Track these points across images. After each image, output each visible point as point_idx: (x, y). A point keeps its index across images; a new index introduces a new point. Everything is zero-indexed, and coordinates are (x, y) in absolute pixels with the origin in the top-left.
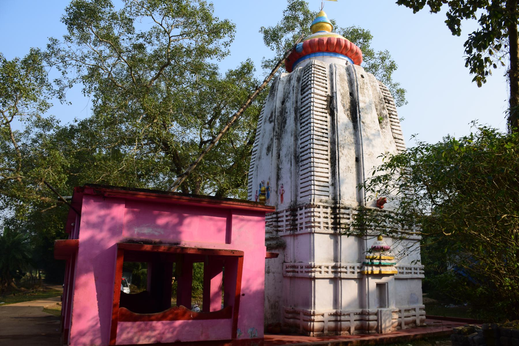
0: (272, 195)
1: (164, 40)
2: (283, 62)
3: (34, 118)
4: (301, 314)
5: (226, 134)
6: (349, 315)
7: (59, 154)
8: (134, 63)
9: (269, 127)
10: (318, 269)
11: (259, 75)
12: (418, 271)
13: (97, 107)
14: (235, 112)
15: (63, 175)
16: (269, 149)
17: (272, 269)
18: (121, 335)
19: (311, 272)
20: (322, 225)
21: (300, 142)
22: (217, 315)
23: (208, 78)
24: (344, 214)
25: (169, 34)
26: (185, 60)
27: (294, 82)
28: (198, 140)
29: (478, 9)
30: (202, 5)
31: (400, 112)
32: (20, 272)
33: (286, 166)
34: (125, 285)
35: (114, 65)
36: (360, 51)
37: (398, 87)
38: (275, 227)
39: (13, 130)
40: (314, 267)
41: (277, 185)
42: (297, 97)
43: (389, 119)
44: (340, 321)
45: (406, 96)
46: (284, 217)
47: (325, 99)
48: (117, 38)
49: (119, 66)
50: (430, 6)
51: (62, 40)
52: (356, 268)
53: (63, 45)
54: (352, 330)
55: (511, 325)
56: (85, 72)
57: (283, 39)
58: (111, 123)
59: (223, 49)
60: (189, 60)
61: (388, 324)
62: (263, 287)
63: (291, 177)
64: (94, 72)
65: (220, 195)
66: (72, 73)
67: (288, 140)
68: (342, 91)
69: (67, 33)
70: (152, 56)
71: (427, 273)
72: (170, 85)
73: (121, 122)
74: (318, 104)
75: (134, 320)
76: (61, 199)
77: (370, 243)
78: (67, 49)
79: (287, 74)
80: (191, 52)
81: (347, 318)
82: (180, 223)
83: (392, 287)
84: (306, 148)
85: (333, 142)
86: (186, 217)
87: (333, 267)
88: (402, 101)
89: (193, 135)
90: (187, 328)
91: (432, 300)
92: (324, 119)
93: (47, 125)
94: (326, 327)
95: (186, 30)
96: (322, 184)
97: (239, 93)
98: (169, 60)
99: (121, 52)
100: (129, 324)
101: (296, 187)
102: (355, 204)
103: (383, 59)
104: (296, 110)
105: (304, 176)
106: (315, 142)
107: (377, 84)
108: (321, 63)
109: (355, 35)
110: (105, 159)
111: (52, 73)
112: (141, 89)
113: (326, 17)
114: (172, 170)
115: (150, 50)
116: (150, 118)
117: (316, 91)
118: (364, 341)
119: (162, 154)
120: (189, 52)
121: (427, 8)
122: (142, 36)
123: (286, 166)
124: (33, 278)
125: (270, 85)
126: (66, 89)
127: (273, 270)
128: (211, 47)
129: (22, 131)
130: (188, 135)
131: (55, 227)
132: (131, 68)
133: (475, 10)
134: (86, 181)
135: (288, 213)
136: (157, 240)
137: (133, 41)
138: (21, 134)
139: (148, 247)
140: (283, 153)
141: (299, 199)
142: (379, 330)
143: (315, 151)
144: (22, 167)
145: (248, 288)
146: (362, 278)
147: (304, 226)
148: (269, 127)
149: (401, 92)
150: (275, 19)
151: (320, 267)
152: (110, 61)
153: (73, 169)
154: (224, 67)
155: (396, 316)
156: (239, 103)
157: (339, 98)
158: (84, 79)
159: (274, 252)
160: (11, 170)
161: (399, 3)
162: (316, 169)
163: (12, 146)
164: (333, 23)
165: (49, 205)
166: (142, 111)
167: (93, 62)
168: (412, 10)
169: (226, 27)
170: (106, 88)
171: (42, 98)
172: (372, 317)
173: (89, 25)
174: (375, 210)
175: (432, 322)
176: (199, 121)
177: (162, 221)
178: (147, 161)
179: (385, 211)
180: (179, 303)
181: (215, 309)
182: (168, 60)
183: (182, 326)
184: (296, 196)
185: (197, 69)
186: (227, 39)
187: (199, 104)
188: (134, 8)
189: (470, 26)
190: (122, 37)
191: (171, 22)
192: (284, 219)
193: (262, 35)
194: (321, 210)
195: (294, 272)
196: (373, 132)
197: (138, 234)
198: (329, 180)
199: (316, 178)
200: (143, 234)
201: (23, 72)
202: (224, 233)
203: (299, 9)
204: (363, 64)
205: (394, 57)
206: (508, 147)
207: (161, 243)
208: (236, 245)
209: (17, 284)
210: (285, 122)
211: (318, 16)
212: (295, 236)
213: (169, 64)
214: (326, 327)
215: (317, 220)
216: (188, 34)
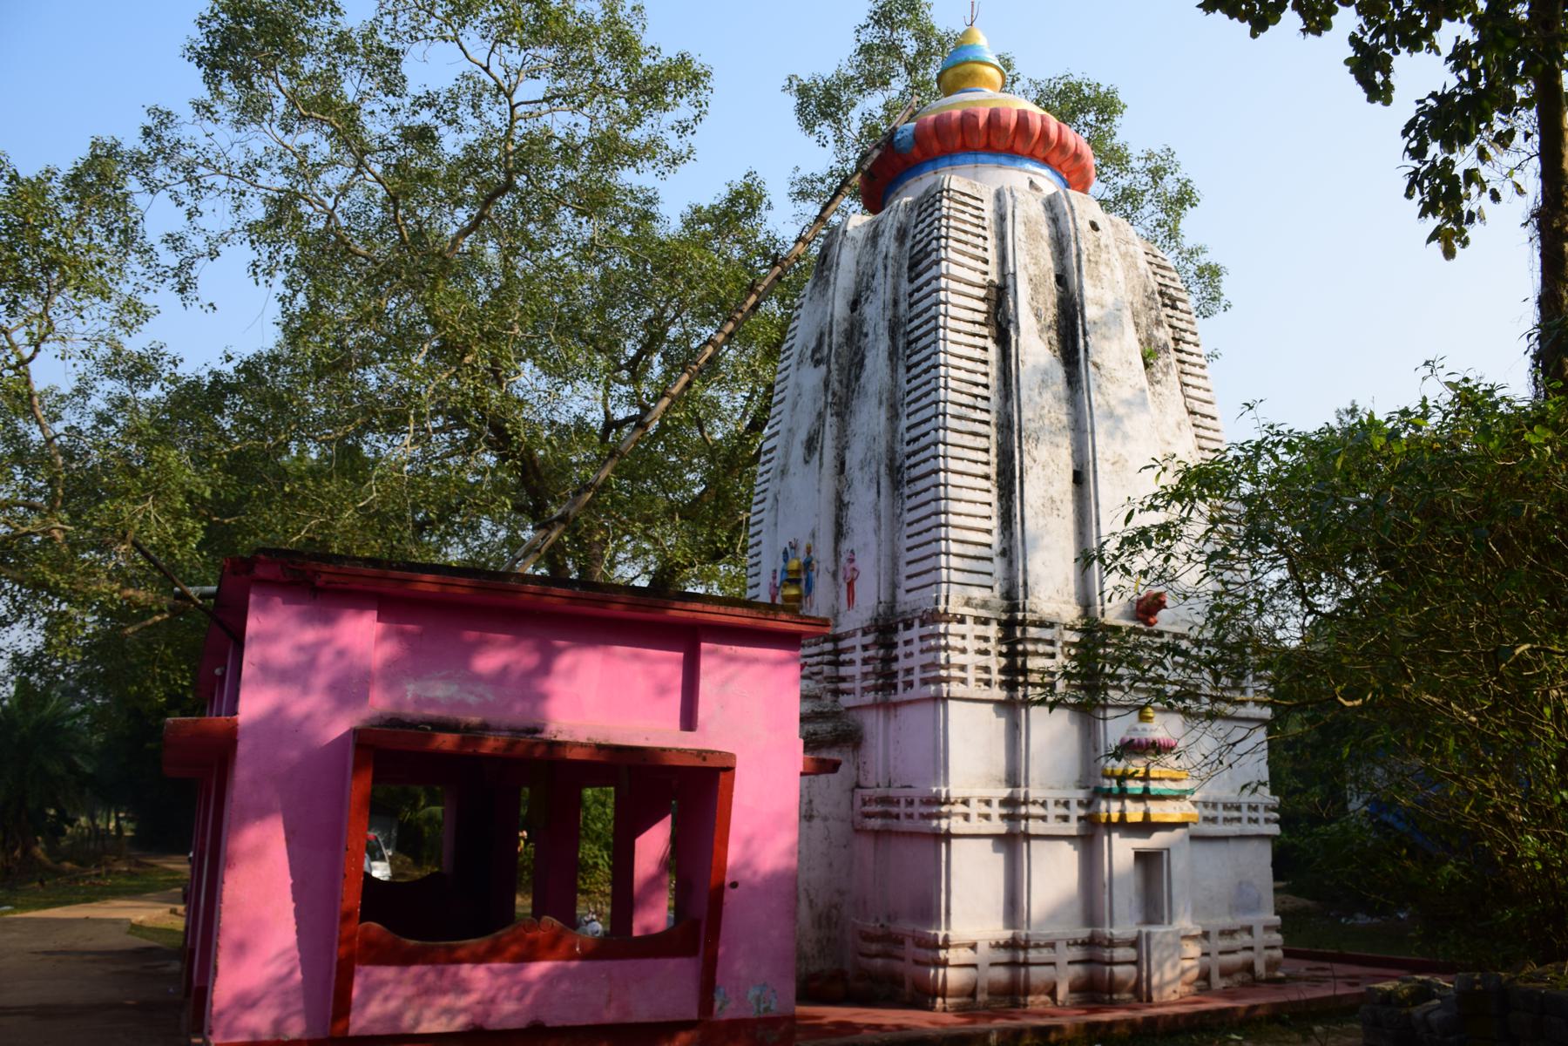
2: (856, 181)
3: (104, 351)
4: (909, 943)
6: (1052, 945)
7: (177, 457)
8: (405, 184)
9: (811, 377)
10: (960, 808)
11: (783, 221)
12: (1261, 814)
14: (709, 331)
15: (189, 523)
16: (811, 445)
17: (820, 808)
18: (364, 1005)
19: (939, 816)
20: (971, 675)
21: (904, 423)
22: (655, 946)
23: (626, 231)
24: (1037, 641)
25: (509, 96)
26: (558, 175)
27: (888, 243)
28: (596, 418)
31: (1207, 333)
32: (61, 813)
33: (864, 498)
34: (376, 856)
35: (344, 191)
36: (1087, 151)
37: (1203, 260)
38: (830, 679)
40: (947, 801)
41: (837, 553)
42: (896, 288)
43: (1174, 356)
44: (1026, 964)
45: (1227, 285)
46: (858, 650)
47: (982, 293)
48: (354, 108)
49: (357, 194)
50: (1302, 14)
51: (186, 113)
52: (1073, 804)
53: (190, 129)
54: (1062, 991)
55: (1541, 978)
57: (855, 114)
59: (673, 142)
60: (571, 175)
61: (1169, 973)
62: (794, 862)
63: (877, 531)
64: (283, 209)
65: (665, 583)
66: (217, 214)
67: (870, 418)
68: (1032, 270)
69: (204, 93)
72: (514, 251)
73: (365, 363)
74: (960, 308)
75: (404, 959)
76: (183, 596)
77: (1117, 728)
78: (202, 142)
79: (868, 218)
80: (576, 150)
81: (1045, 955)
82: (545, 669)
83: (1183, 864)
84: (923, 442)
85: (1007, 427)
86: (561, 651)
87: (1004, 803)
88: (1212, 300)
89: (582, 402)
90: (565, 986)
91: (1301, 902)
92: (978, 354)
93: (141, 369)
94: (983, 983)
95: (562, 83)
96: (971, 550)
97: (722, 276)
98: (509, 174)
100: (388, 973)
101: (894, 559)
102: (1070, 612)
103: (1156, 174)
104: (894, 328)
105: (916, 528)
106: (951, 423)
107: (1139, 248)
108: (971, 185)
109: (1072, 101)
110: (316, 473)
111: (157, 215)
112: (423, 263)
113: (985, 45)
114: (518, 509)
115: (451, 144)
118: (1098, 1024)
119: (490, 459)
120: (569, 152)
121: (1291, 19)
122: (429, 101)
123: (864, 498)
124: (100, 835)
125: (815, 250)
126: (200, 263)
127: (823, 810)
128: (638, 135)
130: (568, 400)
132: (394, 199)
133: (1435, 25)
134: (259, 540)
135: (870, 639)
136: (475, 719)
137: (401, 117)
138: (62, 398)
139: (447, 741)
140: (854, 457)
141: (901, 596)
142: (1141, 992)
143: (952, 451)
144: (69, 496)
145: (747, 864)
146: (1090, 835)
147: (916, 676)
148: (811, 377)
149: (1211, 274)
150: (830, 54)
151: (965, 802)
152: (333, 178)
153: (220, 505)
154: (677, 195)
155: (1193, 950)
156: (722, 304)
158: (256, 232)
159: (832, 755)
160: (32, 508)
163: (36, 436)
165: (146, 611)
166: (429, 330)
167: (281, 182)
168: (1247, 26)
169: (684, 77)
170: (321, 259)
171: (127, 289)
172: (1120, 953)
173: (268, 68)
174: (1133, 630)
175: (1301, 967)
176: (601, 360)
177: (489, 661)
178: (444, 480)
179: (1160, 634)
180: (539, 910)
181: (647, 929)
182: (506, 176)
183: (549, 979)
184: (894, 586)
185: (594, 201)
187: (601, 308)
188: (403, 18)
189: (1422, 75)
190: (368, 106)
191: (515, 59)
192: (858, 655)
193: (793, 101)
194: (970, 628)
195: (885, 815)
196: (1127, 393)
197: (417, 700)
198: (995, 539)
199: (953, 534)
200: (432, 702)
201: (68, 211)
202: (676, 699)
203: (903, 23)
204: (1097, 187)
205: (1190, 167)
206: (1534, 440)
207: (485, 727)
208: (712, 736)
210: (861, 365)
211: (962, 43)
212: (889, 707)
213: (509, 186)
214: (983, 983)
215: (956, 658)
216: (568, 97)
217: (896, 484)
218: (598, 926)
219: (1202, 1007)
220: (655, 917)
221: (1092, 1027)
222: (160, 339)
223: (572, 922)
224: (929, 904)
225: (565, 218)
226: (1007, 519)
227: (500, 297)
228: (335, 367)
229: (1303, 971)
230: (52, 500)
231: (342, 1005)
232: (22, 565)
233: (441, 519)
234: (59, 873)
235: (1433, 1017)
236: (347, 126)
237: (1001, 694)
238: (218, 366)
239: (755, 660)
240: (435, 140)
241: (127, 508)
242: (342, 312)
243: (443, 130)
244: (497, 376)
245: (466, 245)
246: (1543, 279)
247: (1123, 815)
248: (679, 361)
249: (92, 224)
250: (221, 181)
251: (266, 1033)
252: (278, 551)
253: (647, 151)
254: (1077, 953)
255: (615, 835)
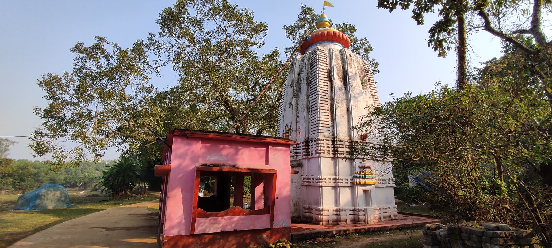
0: (293, 133)
2: (299, 48)
3: (141, 86)
4: (314, 210)
5: (264, 95)
6: (345, 211)
7: (157, 108)
8: (204, 51)
9: (290, 90)
10: (324, 180)
11: (283, 57)
13: (181, 79)
14: (268, 81)
17: (294, 181)
18: (198, 227)
19: (320, 182)
20: (326, 152)
21: (310, 99)
22: (260, 212)
23: (251, 60)
25: (225, 32)
27: (306, 61)
28: (245, 99)
29: (435, 5)
30: (246, 12)
34: (200, 191)
35: (191, 52)
39: (126, 95)
41: (296, 127)
42: (308, 71)
43: (368, 83)
46: (301, 147)
48: (193, 35)
49: (194, 53)
52: (349, 180)
53: (158, 39)
54: (348, 222)
56: (173, 56)
57: (298, 34)
59: (260, 41)
60: (239, 49)
61: (372, 218)
63: (305, 122)
66: (164, 56)
67: (303, 98)
69: (160, 31)
70: (215, 46)
71: (397, 183)
72: (227, 65)
73: (197, 88)
74: (322, 74)
75: (207, 216)
76: (159, 139)
78: (161, 41)
79: (301, 56)
82: (236, 153)
83: (374, 193)
85: (332, 99)
86: (240, 150)
87: (334, 179)
88: (376, 71)
89: (243, 96)
91: (399, 201)
92: (325, 84)
93: (149, 91)
94: (331, 219)
95: (237, 29)
97: (271, 69)
98: (226, 49)
99: (195, 44)
101: (309, 128)
102: (347, 138)
103: (363, 44)
105: (313, 121)
106: (320, 99)
108: (323, 48)
109: (349, 29)
111: (151, 56)
112: (208, 68)
113: (326, 17)
114: (230, 118)
115: (214, 42)
116: (215, 86)
117: (320, 66)
119: (224, 108)
120: (239, 44)
121: (399, 7)
122: (209, 33)
123: (302, 115)
124: (140, 188)
125: (290, 63)
126: (161, 67)
128: (253, 40)
130: (238, 95)
131: (155, 155)
135: (304, 144)
137: (203, 37)
138: (131, 97)
139: (216, 169)
140: (299, 107)
141: (310, 135)
142: (366, 222)
143: (320, 105)
144: (134, 117)
146: (353, 186)
147: (314, 152)
148: (290, 90)
150: (293, 21)
153: (167, 119)
154: (261, 53)
155: (377, 212)
158: (174, 60)
159: (297, 169)
160: (126, 120)
161: (381, 5)
162: (321, 116)
163: (126, 104)
164: (331, 21)
165: (151, 141)
166: (210, 81)
167: (178, 50)
168: (389, 10)
169: (262, 27)
170: (187, 67)
172: (361, 213)
174: (361, 142)
175: (402, 216)
176: (246, 87)
177: (225, 152)
178: (215, 113)
179: (367, 143)
180: (235, 204)
181: (258, 208)
182: (225, 48)
184: (309, 133)
185: (244, 54)
186: (262, 34)
187: (246, 76)
189: (433, 17)
192: (301, 148)
194: (325, 142)
195: (308, 182)
196: (358, 92)
198: (330, 123)
199: (321, 122)
203: (308, 14)
204: (350, 47)
205: (371, 42)
209: (131, 192)
210: (301, 87)
211: (322, 17)
212: (308, 159)
214: (331, 219)
215: (322, 148)
216: (238, 32)
217: (309, 112)
221: (356, 230)
224: (318, 202)
225: (238, 57)
226: (332, 119)
227: (225, 75)
228: (191, 89)
229: (402, 217)
230: (130, 118)
231: (193, 229)
232: (124, 132)
236: (191, 38)
237: (333, 156)
239: (281, 150)
241: (147, 120)
244: (225, 91)
245: (217, 64)
246: (459, 60)
247: (360, 182)
248: (263, 87)
250: (165, 50)
252: (180, 129)
253: (255, 43)
254: (351, 213)
255: (251, 186)
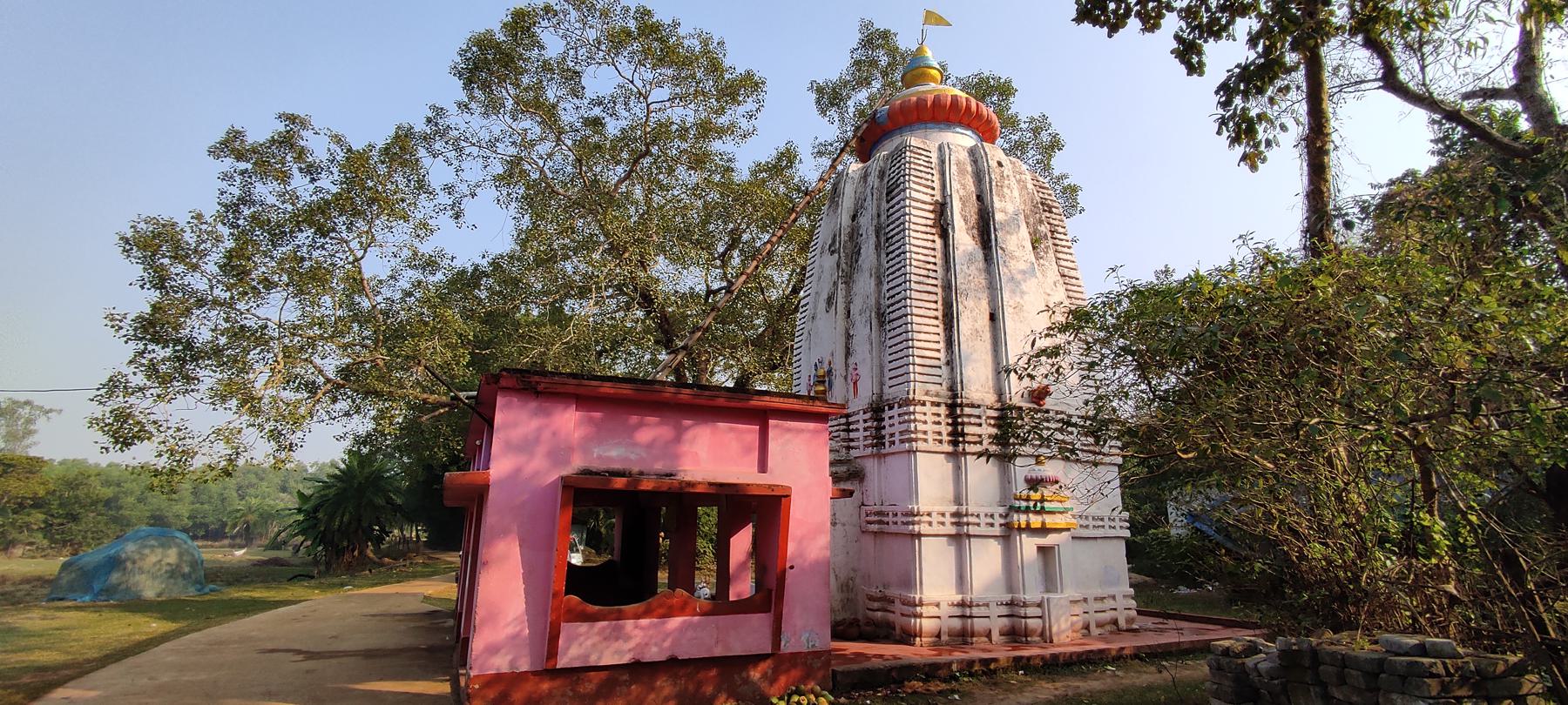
0: (838, 383)
1: (638, 110)
2: (853, 143)
3: (406, 253)
4: (897, 602)
7: (453, 314)
8: (587, 152)
9: (829, 261)
10: (926, 518)
11: (809, 170)
12: (1117, 524)
16: (830, 301)
17: (841, 518)
18: (568, 648)
19: (913, 523)
20: (930, 437)
21: (886, 287)
22: (743, 607)
23: (717, 178)
24: (970, 416)
26: (675, 147)
27: (873, 180)
28: (701, 289)
29: (1238, 20)
30: (705, 43)
31: (1072, 226)
32: (382, 530)
33: (862, 332)
34: (573, 548)
35: (550, 156)
36: (994, 117)
37: (1066, 182)
38: (844, 440)
41: (847, 365)
42: (879, 207)
43: (1051, 242)
46: (861, 422)
48: (554, 106)
49: (558, 157)
50: (1141, 20)
53: (455, 119)
54: (995, 636)
55: (1339, 642)
56: (499, 169)
57: (850, 103)
58: (546, 260)
59: (744, 124)
60: (684, 146)
62: (828, 553)
65: (742, 385)
67: (865, 285)
68: (962, 192)
70: (616, 140)
71: (1133, 527)
73: (566, 258)
74: (918, 217)
77: (1022, 469)
78: (463, 127)
80: (687, 130)
81: (982, 611)
82: (678, 439)
84: (897, 298)
85: (947, 287)
87: (954, 515)
88: (1072, 207)
89: (694, 279)
90: (690, 634)
92: (929, 244)
93: (430, 264)
97: (776, 203)
98: (647, 145)
100: (583, 627)
101: (882, 368)
102: (991, 399)
103: (1036, 131)
104: (878, 231)
106: (914, 286)
108: (923, 143)
109: (985, 88)
110: (538, 324)
111: (438, 172)
112: (597, 199)
114: (657, 342)
115: (613, 128)
117: (914, 194)
118: (1021, 658)
119: (640, 314)
120: (683, 132)
121: (1134, 23)
123: (862, 332)
124: (405, 540)
125: (829, 187)
126: (465, 200)
127: (843, 520)
128: (723, 120)
129: (383, 277)
130: (681, 278)
132: (580, 161)
133: (1231, 22)
134: (505, 362)
135: (868, 416)
136: (636, 469)
137: (582, 111)
138: (381, 282)
139: (619, 483)
140: (855, 309)
141: (886, 389)
142: (1046, 637)
143: (915, 303)
144: (386, 339)
146: (1008, 534)
147: (897, 438)
148: (829, 261)
149: (1072, 191)
150: (835, 67)
151: (929, 515)
152: (544, 148)
153: (479, 343)
154: (746, 157)
156: (774, 220)
157: (957, 205)
159: (847, 486)
162: (916, 336)
164: (943, 68)
167: (513, 151)
168: (1106, 29)
169: (750, 84)
170: (538, 197)
172: (1031, 611)
173: (502, 80)
175: (1149, 622)
176: (705, 255)
179: (1047, 411)
180: (672, 585)
182: (645, 145)
183: (682, 629)
184: (882, 384)
185: (698, 161)
186: (750, 105)
187: (705, 222)
188: (582, 51)
189: (1228, 53)
190: (562, 105)
191: (649, 76)
192: (861, 426)
193: (814, 96)
194: (928, 409)
195: (880, 522)
196: (1022, 266)
197: (600, 457)
198: (942, 355)
199: (916, 352)
200: (611, 459)
201: (382, 169)
204: (999, 141)
205: (1057, 126)
206: (1320, 284)
209: (377, 551)
210: (859, 253)
211: (918, 55)
212: (881, 456)
213: (648, 153)
215: (921, 427)
217: (882, 324)
218: (707, 591)
219: (1088, 648)
220: (743, 587)
221: (1017, 659)
222: (441, 245)
223: (691, 589)
225: (681, 171)
226: (949, 343)
227: (644, 219)
228: (548, 260)
230: (376, 342)
231: (553, 652)
233: (612, 349)
234: (383, 565)
235: (1263, 666)
236: (548, 115)
237: (950, 449)
238: (479, 261)
240: (603, 125)
242: (551, 229)
243: (608, 119)
244: (643, 265)
247: (1028, 524)
248: (751, 254)
249: (399, 178)
250: (475, 150)
251: (505, 669)
253: (730, 129)
254: (1004, 610)
